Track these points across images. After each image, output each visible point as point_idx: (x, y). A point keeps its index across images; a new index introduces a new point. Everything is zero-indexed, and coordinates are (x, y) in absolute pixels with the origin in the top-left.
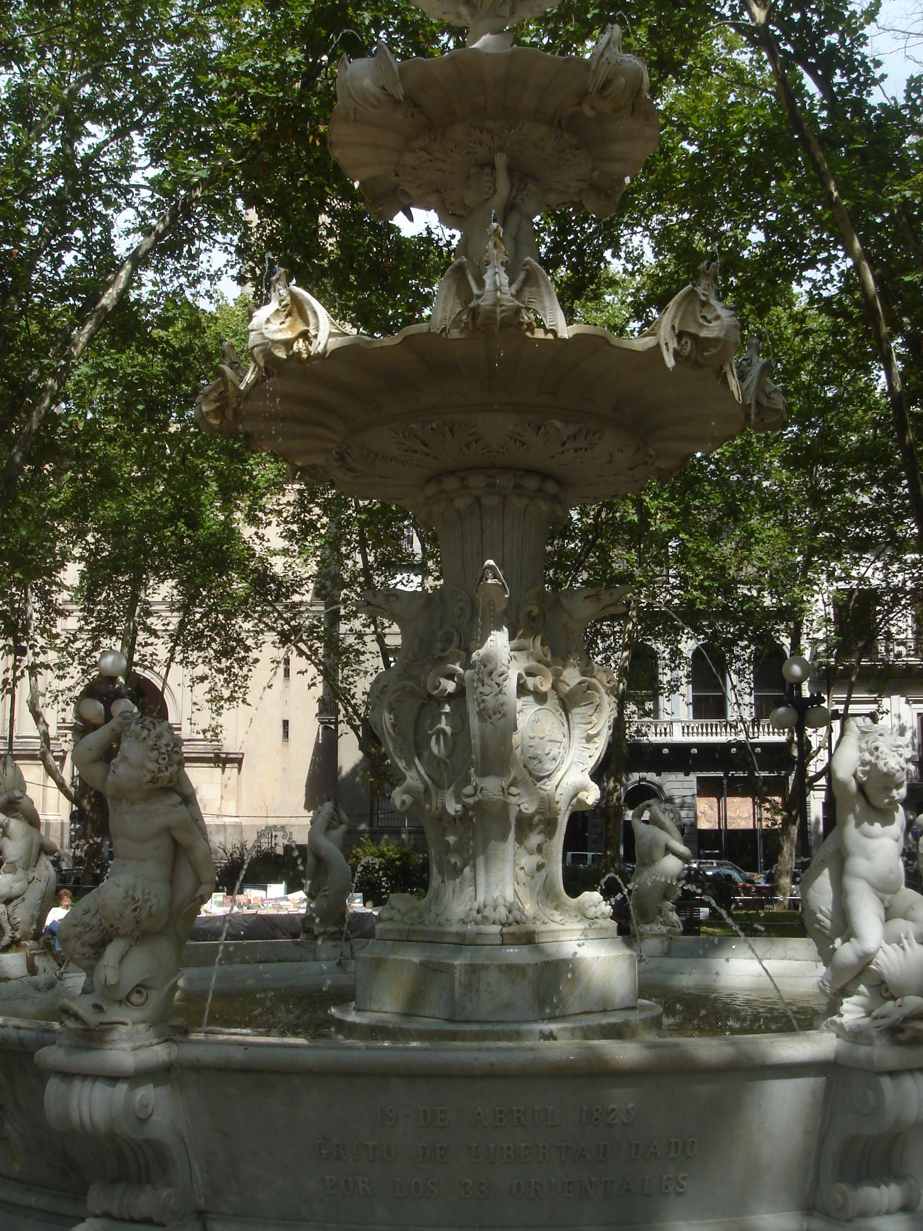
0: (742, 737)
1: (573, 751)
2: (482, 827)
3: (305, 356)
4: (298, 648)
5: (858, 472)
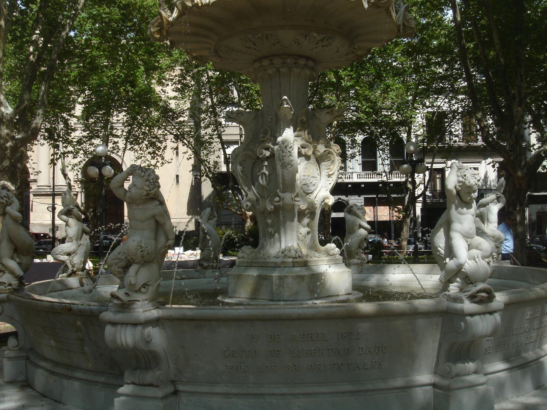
0: (385, 179)
1: (322, 181)
2: (282, 216)
3: (200, 5)
4: (183, 142)
5: (437, 58)
